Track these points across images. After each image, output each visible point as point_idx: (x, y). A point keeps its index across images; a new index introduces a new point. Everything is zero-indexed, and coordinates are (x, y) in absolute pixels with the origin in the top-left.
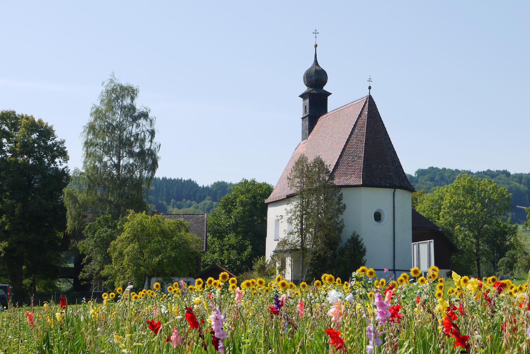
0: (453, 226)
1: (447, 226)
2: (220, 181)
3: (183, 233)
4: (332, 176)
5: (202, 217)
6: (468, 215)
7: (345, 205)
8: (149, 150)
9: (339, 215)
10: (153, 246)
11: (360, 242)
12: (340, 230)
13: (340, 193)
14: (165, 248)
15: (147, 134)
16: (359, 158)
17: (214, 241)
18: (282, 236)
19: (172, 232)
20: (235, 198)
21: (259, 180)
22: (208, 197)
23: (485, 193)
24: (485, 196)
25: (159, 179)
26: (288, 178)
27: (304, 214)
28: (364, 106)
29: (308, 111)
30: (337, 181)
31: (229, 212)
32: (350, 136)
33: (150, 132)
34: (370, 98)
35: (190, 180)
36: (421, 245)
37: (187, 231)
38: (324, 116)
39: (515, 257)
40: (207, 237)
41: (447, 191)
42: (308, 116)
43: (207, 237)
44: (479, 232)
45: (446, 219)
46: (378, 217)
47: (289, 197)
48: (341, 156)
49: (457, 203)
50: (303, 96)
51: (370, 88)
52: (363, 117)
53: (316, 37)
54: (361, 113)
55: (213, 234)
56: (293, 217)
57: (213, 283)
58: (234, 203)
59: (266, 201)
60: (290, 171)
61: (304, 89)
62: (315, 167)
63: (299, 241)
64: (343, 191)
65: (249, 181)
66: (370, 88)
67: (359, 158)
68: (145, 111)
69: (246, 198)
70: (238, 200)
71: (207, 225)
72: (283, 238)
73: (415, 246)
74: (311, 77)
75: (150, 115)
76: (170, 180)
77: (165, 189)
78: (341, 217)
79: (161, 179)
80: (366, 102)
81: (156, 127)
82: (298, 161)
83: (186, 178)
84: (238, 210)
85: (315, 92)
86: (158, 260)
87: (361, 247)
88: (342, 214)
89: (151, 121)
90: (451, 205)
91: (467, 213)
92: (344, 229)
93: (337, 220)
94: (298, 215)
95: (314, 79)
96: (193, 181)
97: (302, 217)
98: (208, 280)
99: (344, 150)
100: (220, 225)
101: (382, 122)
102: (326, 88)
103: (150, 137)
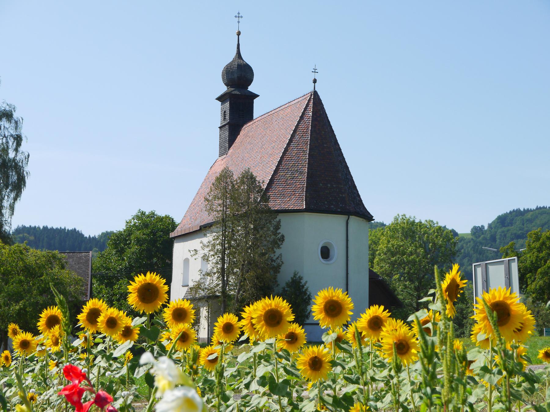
0: (390, 275)
1: (383, 275)
2: (109, 231)
3: (56, 270)
4: (265, 197)
5: (85, 257)
6: (409, 262)
7: (283, 236)
8: (14, 160)
9: (275, 249)
10: (12, 287)
11: (303, 286)
12: (277, 269)
13: (277, 219)
14: (29, 291)
15: (11, 141)
16: (301, 173)
17: (101, 289)
18: (194, 277)
19: (39, 268)
20: (129, 235)
21: (161, 213)
22: (95, 249)
23: (428, 237)
24: (428, 240)
25: (39, 228)
26: (207, 200)
27: (225, 251)
28: (307, 105)
29: (227, 117)
30: (274, 204)
31: (121, 252)
32: (289, 144)
33: (15, 139)
34: (315, 94)
35: (75, 229)
36: (491, 268)
37: (63, 267)
38: (248, 124)
39: (465, 312)
40: (92, 284)
41: (382, 234)
42: (228, 124)
43: (92, 284)
44: (420, 283)
45: (382, 267)
46: (326, 253)
47: (203, 229)
48: (276, 172)
49: (396, 248)
50: (221, 99)
51: (315, 81)
52: (306, 119)
53: (239, 22)
54: (303, 114)
55: (100, 280)
56: (212, 253)
57: (101, 319)
58: (127, 240)
59: (172, 235)
60: (209, 190)
61: (223, 89)
62: (244, 183)
63: (219, 285)
64: (280, 217)
65: (147, 213)
66: (315, 81)
67: (301, 173)
68: (8, 108)
69: (144, 234)
70: (132, 237)
71: (92, 269)
72: (197, 280)
73: (479, 270)
74: (232, 73)
75: (16, 115)
76: (52, 229)
77: (46, 239)
78: (278, 252)
79: (41, 228)
80: (309, 100)
81: (24, 132)
82: (220, 175)
83: (70, 227)
84: (132, 250)
85: (237, 92)
86: (17, 307)
87: (305, 293)
88: (279, 247)
89: (16, 122)
90: (389, 250)
91: (407, 259)
92: (283, 268)
93: (272, 256)
94: (218, 250)
95: (236, 76)
96: (78, 231)
97: (223, 253)
98: (86, 309)
99: (280, 162)
100: (108, 269)
101: (331, 127)
102: (252, 88)
103: (15, 144)
